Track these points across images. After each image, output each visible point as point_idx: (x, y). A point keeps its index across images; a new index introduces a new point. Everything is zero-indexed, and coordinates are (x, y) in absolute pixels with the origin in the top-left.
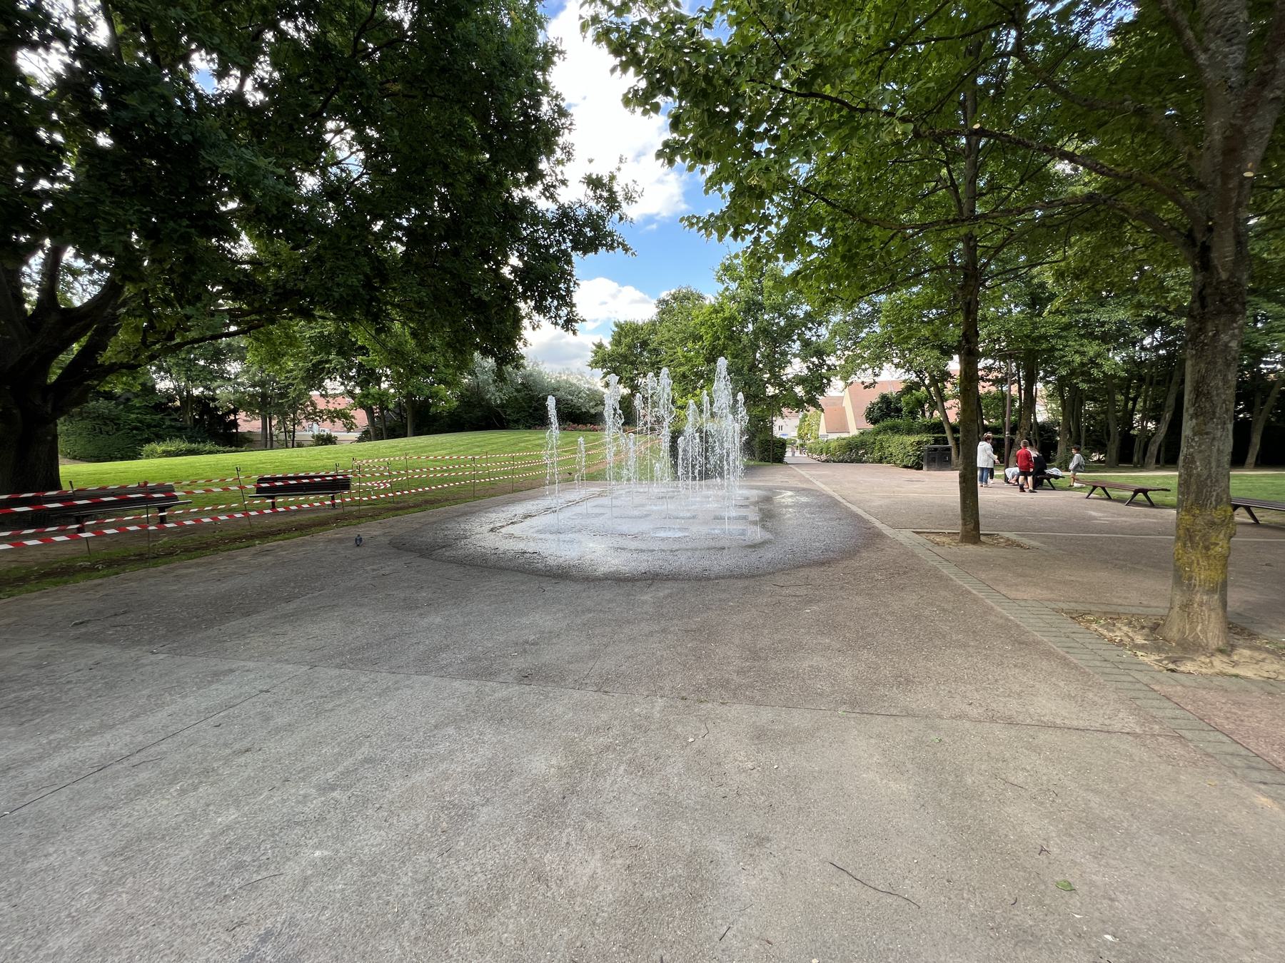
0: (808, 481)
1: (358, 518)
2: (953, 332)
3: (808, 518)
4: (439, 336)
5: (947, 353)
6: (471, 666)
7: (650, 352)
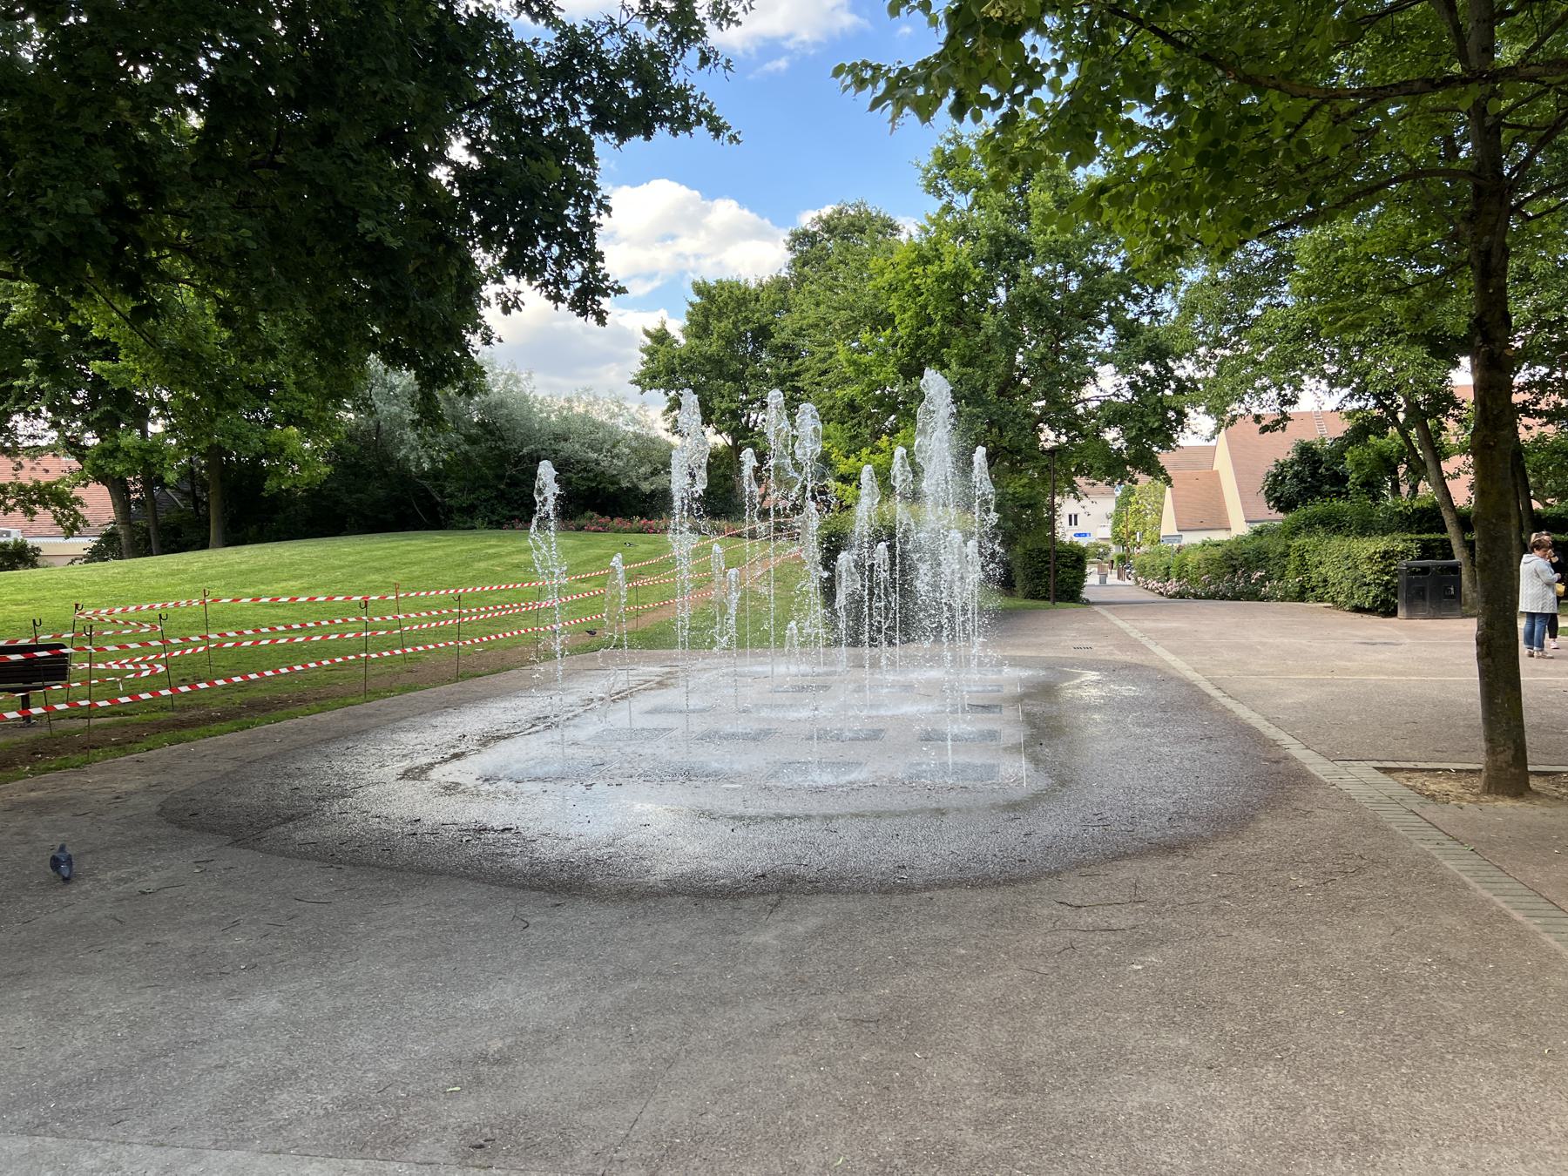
0: (1136, 646)
1: (84, 748)
2: (1456, 313)
3: (1137, 737)
4: (286, 319)
5: (1444, 350)
6: (350, 1122)
7: (774, 351)
